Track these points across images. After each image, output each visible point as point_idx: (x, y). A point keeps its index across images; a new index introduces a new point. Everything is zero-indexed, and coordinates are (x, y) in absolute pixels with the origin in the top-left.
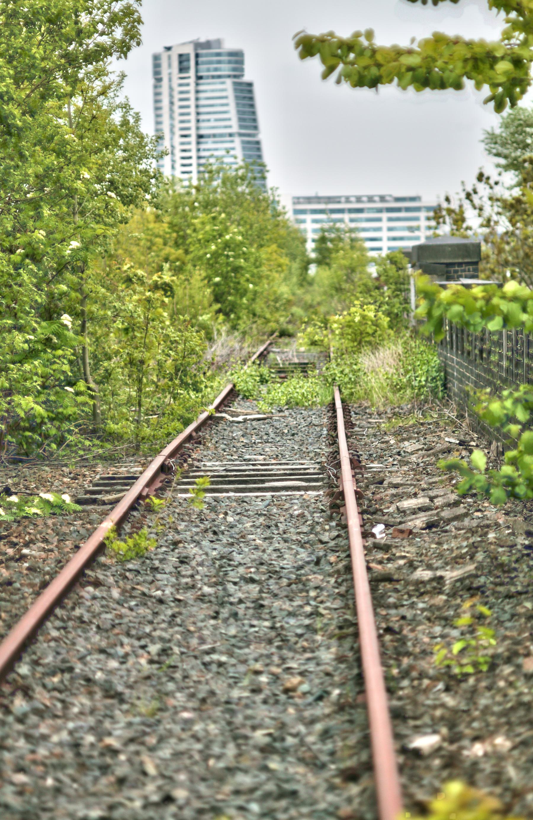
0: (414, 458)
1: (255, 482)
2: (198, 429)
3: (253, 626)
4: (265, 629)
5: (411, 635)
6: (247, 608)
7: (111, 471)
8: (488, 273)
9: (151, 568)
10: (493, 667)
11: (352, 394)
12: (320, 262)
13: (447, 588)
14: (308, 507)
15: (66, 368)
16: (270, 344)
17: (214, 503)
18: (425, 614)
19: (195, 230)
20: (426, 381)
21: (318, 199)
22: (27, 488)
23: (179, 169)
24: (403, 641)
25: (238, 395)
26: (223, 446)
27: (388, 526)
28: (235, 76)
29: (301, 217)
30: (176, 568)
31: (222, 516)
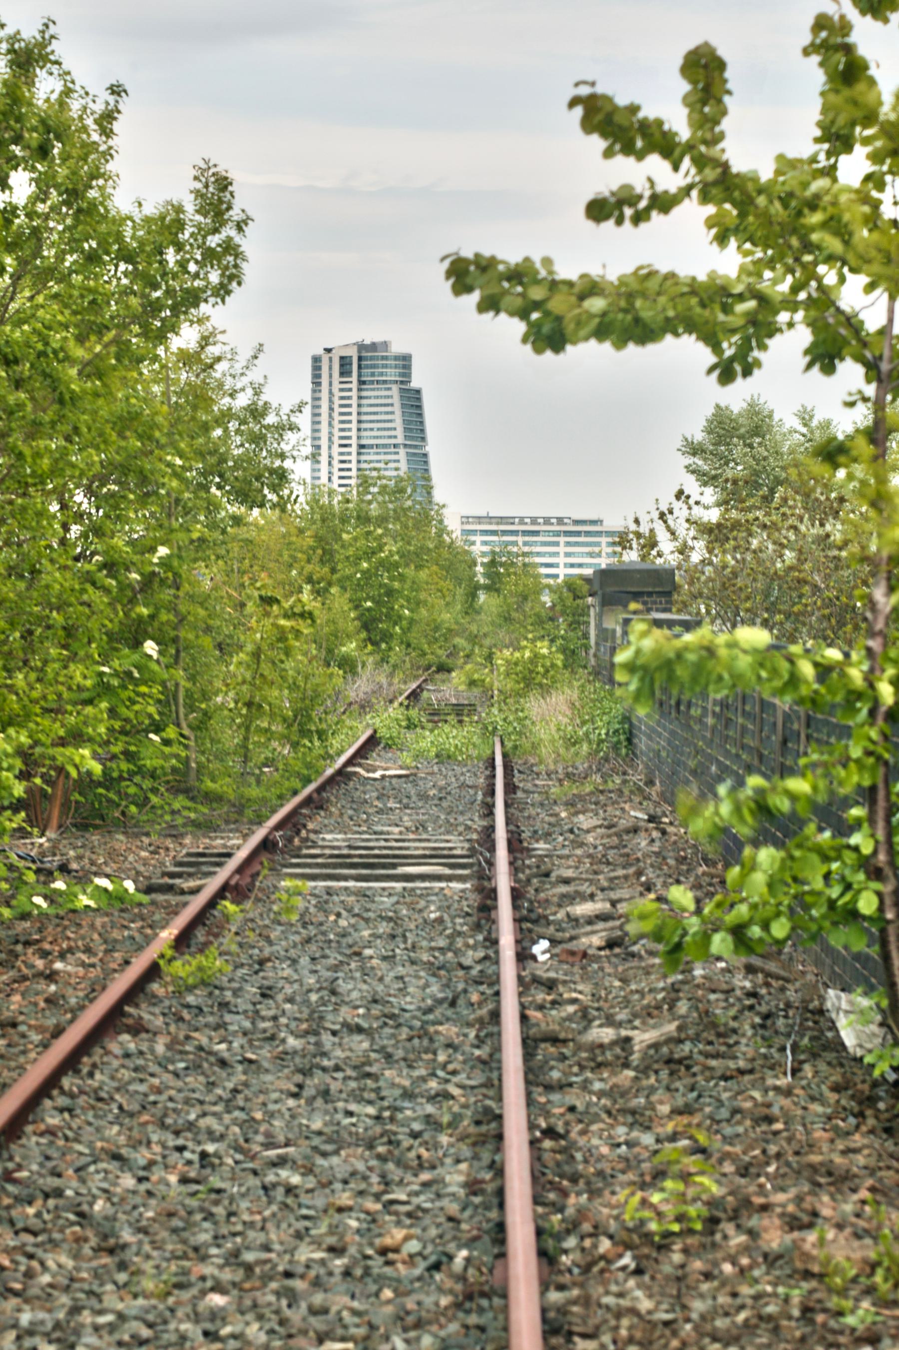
0: (590, 839)
1: (384, 866)
2: (320, 789)
3: (350, 1114)
4: (368, 1120)
5: (582, 1141)
6: (346, 1078)
7: (204, 844)
8: (680, 606)
9: (220, 1004)
10: (712, 1222)
11: (515, 747)
12: (488, 588)
13: (635, 1058)
14: (449, 907)
15: (152, 709)
16: (425, 681)
17: (325, 897)
18: (603, 1101)
19: (343, 547)
20: (607, 734)
21: (489, 519)
22: (93, 863)
23: (336, 481)
24: (567, 1152)
25: (379, 744)
26: (350, 812)
27: (553, 942)
28: (402, 382)
29: (473, 538)
30: (254, 1004)
31: (332, 918)
